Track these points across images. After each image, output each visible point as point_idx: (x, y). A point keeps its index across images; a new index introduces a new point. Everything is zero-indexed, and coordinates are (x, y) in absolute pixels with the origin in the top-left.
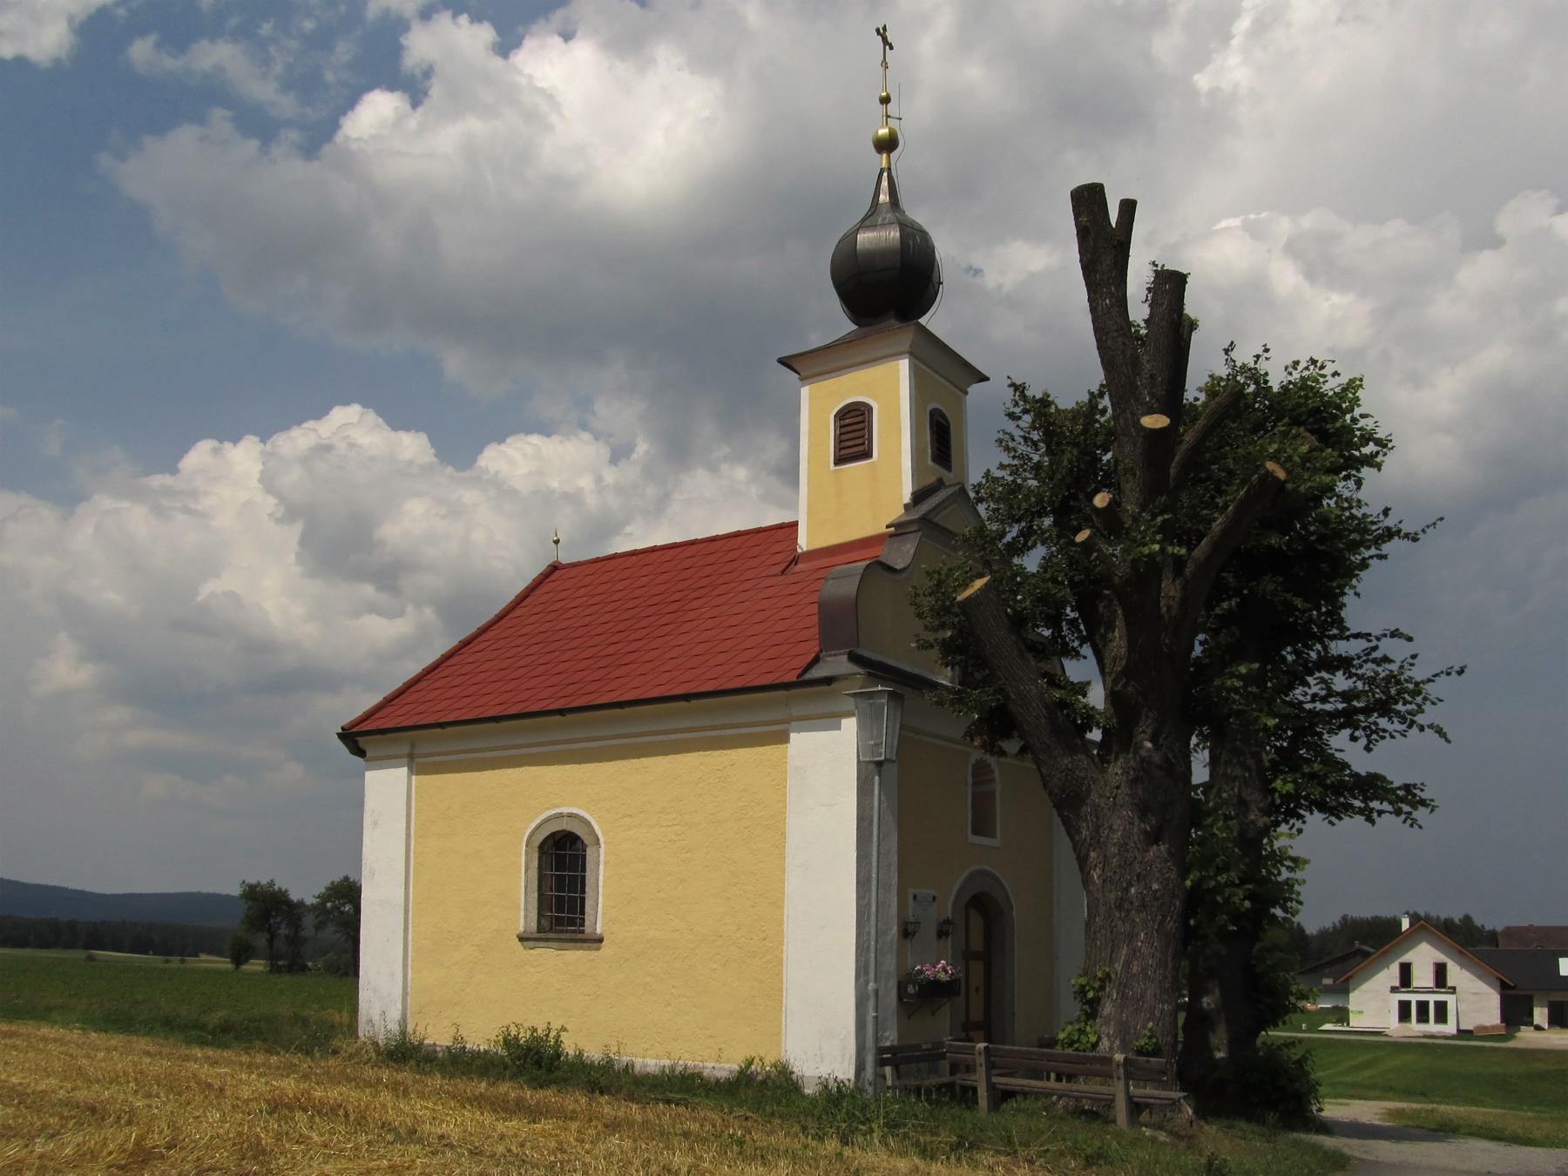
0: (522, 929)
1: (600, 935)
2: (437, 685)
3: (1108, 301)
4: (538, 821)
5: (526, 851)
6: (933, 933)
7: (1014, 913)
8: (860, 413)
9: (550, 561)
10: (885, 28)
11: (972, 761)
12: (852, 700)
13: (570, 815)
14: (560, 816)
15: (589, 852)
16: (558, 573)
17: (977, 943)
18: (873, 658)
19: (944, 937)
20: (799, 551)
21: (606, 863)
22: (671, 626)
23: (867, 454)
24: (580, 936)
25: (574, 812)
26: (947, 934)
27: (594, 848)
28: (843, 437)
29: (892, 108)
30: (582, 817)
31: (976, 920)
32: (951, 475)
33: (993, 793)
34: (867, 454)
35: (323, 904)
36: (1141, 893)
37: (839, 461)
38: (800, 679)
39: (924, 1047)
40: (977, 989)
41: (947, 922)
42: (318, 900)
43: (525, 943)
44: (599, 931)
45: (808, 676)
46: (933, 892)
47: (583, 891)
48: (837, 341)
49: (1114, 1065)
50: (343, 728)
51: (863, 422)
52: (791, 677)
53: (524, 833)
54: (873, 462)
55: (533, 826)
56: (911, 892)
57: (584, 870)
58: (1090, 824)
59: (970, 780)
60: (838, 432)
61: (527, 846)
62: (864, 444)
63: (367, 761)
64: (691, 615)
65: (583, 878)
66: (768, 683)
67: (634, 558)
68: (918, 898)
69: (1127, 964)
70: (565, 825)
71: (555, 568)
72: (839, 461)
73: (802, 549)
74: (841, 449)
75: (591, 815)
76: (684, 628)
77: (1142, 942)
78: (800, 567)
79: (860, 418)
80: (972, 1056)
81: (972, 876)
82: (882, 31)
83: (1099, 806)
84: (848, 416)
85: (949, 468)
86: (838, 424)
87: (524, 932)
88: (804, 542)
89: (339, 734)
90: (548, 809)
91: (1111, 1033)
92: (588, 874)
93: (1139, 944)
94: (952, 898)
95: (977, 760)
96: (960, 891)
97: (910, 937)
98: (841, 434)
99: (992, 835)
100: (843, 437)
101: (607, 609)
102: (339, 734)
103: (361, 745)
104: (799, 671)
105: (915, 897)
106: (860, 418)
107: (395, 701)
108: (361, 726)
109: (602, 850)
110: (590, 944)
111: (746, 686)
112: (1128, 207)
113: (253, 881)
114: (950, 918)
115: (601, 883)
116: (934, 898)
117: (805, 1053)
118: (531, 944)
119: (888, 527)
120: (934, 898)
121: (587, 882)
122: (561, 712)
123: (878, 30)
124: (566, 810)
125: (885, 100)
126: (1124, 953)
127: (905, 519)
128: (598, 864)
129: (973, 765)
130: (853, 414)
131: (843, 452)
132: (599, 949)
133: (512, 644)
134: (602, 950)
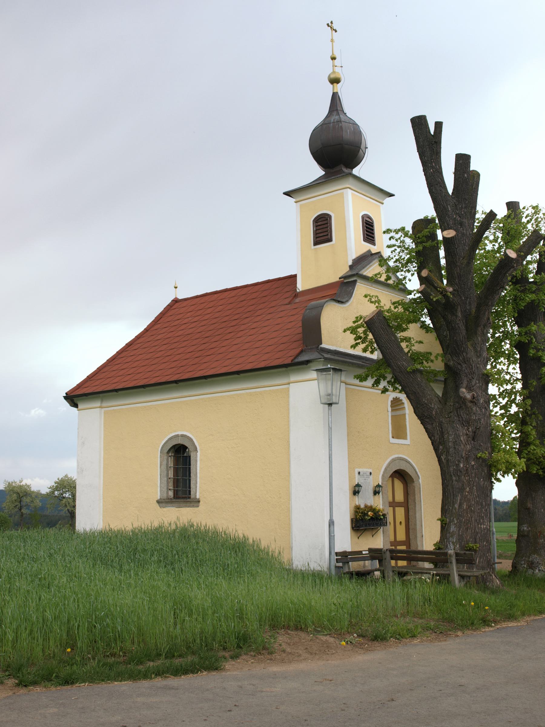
0: (159, 498)
1: (199, 499)
2: (114, 368)
3: (431, 170)
4: (166, 439)
5: (160, 455)
6: (371, 492)
7: (420, 481)
8: (326, 219)
9: (173, 298)
10: (332, 23)
11: (391, 399)
12: (315, 372)
13: (183, 436)
14: (177, 436)
15: (192, 455)
16: (177, 304)
17: (400, 497)
18: (332, 349)
19: (377, 494)
20: (298, 291)
21: (201, 460)
22: (233, 334)
23: (330, 240)
24: (188, 500)
25: (185, 434)
26: (379, 493)
27: (195, 453)
28: (318, 232)
29: (336, 62)
30: (188, 436)
31: (399, 485)
32: (375, 247)
33: (405, 415)
34: (330, 240)
35: (53, 492)
36: (466, 467)
37: (316, 243)
38: (293, 362)
39: (364, 553)
40: (401, 523)
41: (378, 486)
42: (50, 490)
43: (161, 505)
44: (198, 497)
45: (296, 360)
46: (371, 471)
47: (190, 476)
48: (311, 183)
49: (448, 555)
50: (66, 394)
51: (327, 223)
52: (288, 361)
53: (159, 446)
54: (333, 245)
55: (163, 442)
56: (357, 470)
57: (190, 465)
58: (439, 432)
59: (390, 409)
60: (315, 229)
61: (161, 453)
62: (328, 235)
63: (78, 410)
64: (243, 327)
65: (190, 468)
66: (277, 364)
67: (216, 295)
68: (360, 474)
69: (460, 505)
70: (180, 441)
71: (176, 301)
72: (316, 243)
73: (299, 290)
74: (317, 238)
75: (193, 435)
76: (239, 335)
77: (468, 492)
78: (297, 300)
79: (326, 222)
80: (381, 555)
81: (394, 460)
82: (330, 24)
83: (442, 422)
84: (320, 220)
85: (374, 244)
86: (315, 224)
87: (160, 499)
88: (301, 286)
89: (64, 397)
90: (171, 433)
91: (454, 541)
92: (192, 466)
93: (467, 494)
94: (382, 473)
95: (393, 398)
96: (386, 469)
97: (357, 494)
98: (316, 230)
99: (405, 438)
100: (318, 232)
101: (201, 324)
102: (64, 397)
103: (75, 401)
104: (292, 358)
105: (359, 473)
106: (326, 222)
107: (94, 377)
108: (75, 392)
109: (199, 454)
110: (193, 504)
111: (267, 366)
112: (439, 125)
113: (10, 480)
114: (380, 484)
115: (198, 471)
116: (371, 473)
117: (302, 558)
118: (164, 505)
119: (340, 278)
120: (371, 473)
121: (192, 471)
122: (176, 382)
123: (328, 25)
124: (180, 433)
125: (333, 58)
126: (459, 499)
127: (350, 273)
128: (196, 461)
129: (391, 401)
130: (322, 219)
131: (318, 239)
132: (198, 506)
133: (153, 345)
134: (200, 506)
